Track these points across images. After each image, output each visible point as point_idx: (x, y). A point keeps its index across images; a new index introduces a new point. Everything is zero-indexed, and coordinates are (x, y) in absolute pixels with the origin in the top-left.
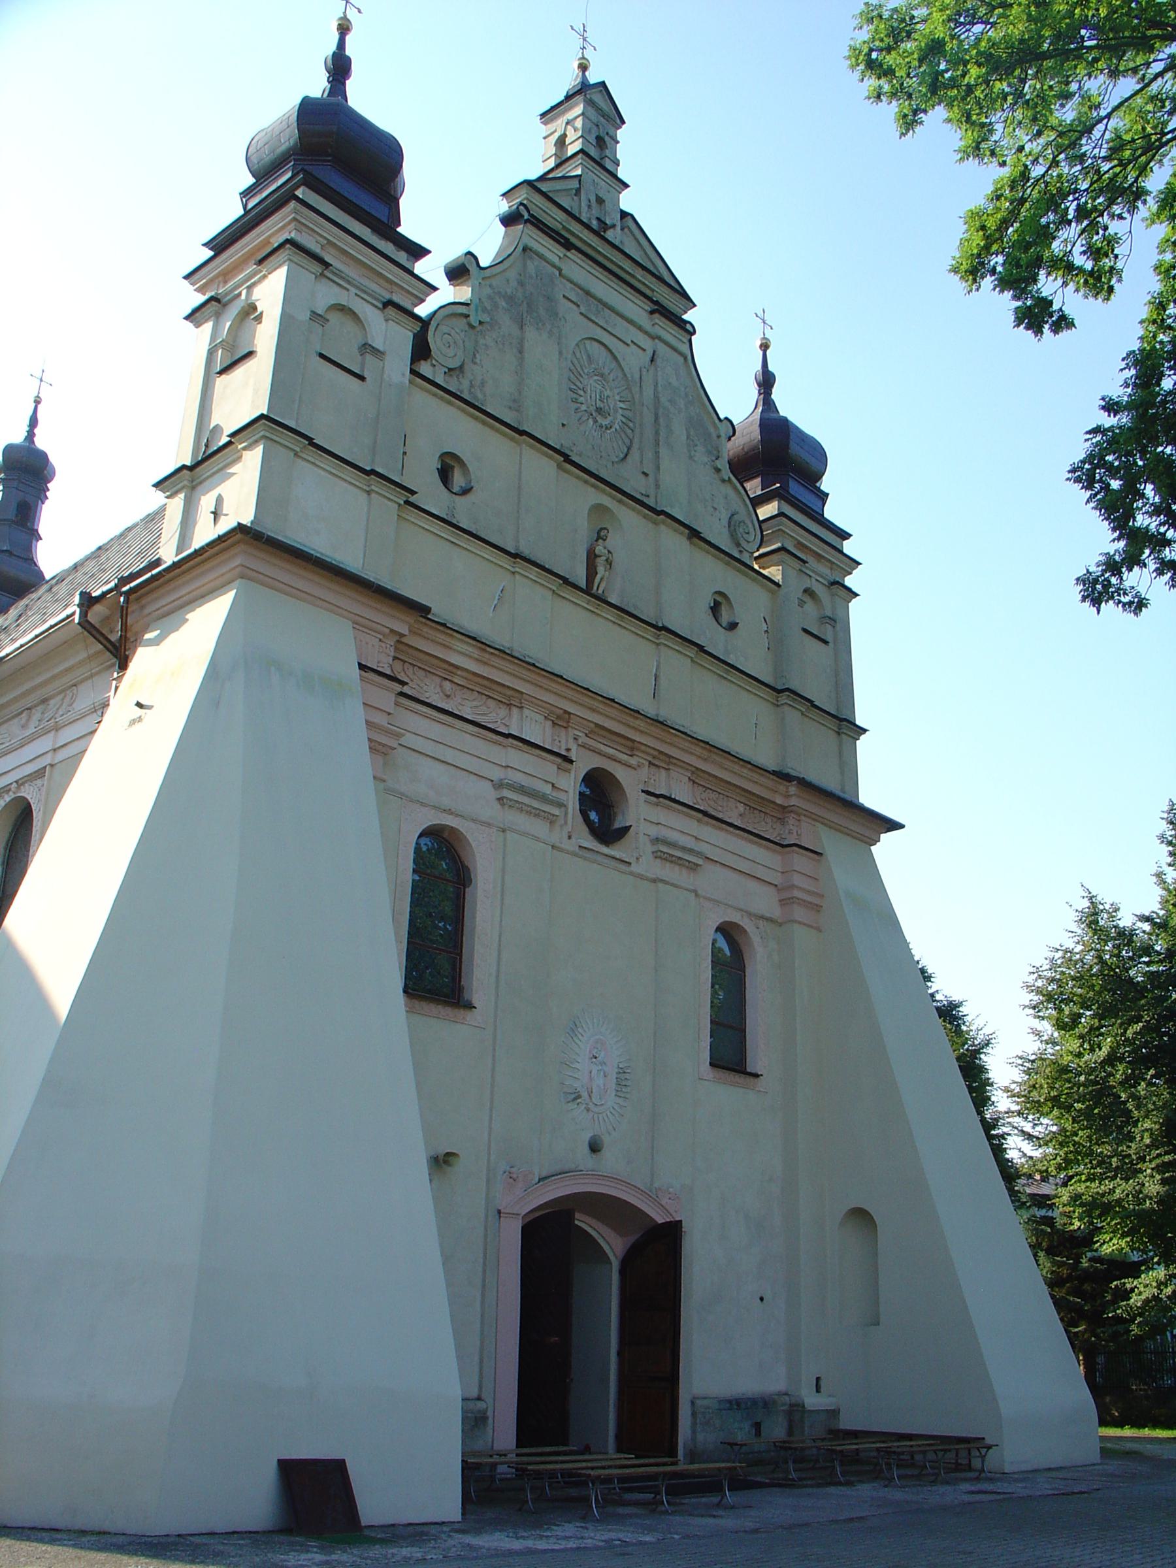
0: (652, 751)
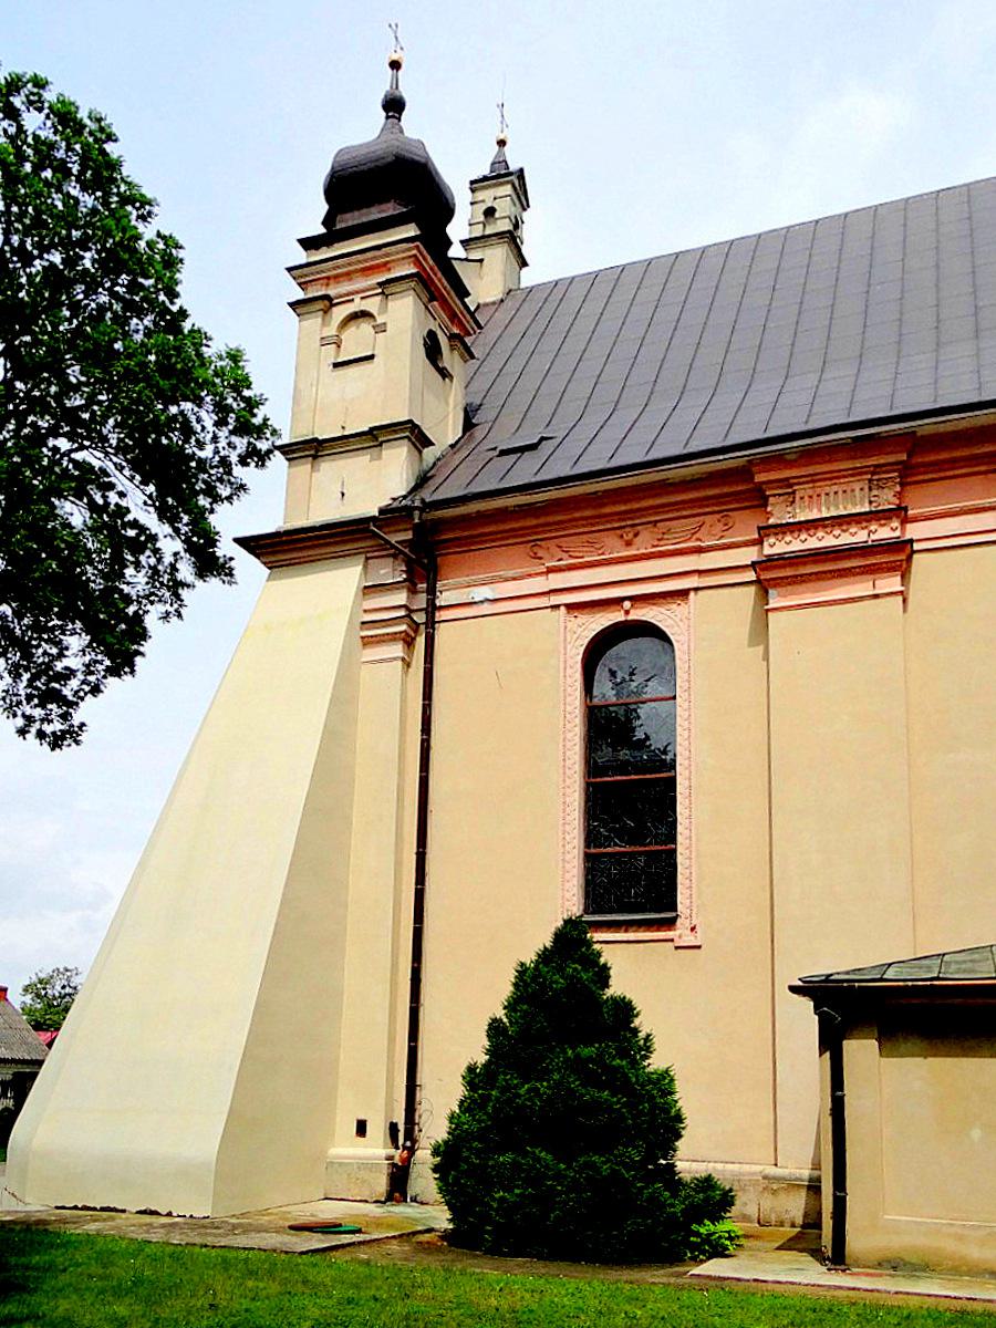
0: (895, 467)
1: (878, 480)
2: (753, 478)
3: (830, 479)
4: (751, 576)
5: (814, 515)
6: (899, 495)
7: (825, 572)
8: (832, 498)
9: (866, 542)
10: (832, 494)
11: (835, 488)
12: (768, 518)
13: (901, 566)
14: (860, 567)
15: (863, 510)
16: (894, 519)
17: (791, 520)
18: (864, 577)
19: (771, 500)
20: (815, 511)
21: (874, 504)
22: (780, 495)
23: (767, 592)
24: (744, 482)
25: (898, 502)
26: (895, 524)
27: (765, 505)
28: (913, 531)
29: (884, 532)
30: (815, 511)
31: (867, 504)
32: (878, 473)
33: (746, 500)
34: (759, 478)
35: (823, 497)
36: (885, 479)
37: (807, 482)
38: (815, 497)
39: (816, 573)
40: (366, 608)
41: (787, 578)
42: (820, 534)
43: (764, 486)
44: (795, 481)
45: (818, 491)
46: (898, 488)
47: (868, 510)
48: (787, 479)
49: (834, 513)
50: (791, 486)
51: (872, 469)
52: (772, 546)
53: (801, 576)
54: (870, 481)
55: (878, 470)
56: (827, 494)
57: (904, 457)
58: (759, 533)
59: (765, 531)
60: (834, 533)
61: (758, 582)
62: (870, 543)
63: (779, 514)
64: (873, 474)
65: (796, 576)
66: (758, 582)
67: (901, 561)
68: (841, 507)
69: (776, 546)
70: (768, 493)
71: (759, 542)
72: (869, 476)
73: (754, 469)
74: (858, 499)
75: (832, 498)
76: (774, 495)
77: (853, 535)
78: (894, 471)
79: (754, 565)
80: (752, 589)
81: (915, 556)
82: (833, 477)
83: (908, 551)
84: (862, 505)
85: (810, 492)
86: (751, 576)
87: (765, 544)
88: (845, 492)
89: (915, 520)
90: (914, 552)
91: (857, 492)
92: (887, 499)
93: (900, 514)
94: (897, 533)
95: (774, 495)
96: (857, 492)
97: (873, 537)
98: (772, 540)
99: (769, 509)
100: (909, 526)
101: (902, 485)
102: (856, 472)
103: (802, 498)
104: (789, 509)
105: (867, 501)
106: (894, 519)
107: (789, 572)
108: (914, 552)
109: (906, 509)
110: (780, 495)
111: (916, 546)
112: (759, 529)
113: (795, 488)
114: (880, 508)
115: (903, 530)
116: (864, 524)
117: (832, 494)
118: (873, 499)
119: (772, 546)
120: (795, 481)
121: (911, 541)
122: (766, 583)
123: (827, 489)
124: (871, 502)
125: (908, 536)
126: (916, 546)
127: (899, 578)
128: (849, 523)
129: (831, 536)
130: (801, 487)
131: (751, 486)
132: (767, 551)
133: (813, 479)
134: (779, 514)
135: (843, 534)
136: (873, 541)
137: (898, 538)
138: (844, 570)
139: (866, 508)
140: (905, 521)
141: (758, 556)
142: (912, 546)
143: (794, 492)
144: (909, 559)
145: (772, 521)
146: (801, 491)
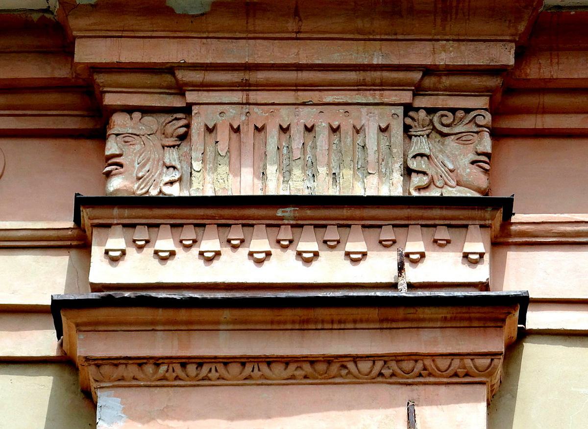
0: (476, 82)
1: (431, 111)
2: (72, 54)
3: (297, 87)
4: (42, 341)
5: (246, 184)
6: (486, 162)
7: (269, 361)
8: (297, 145)
9: (394, 286)
10: (297, 132)
11: (307, 115)
12: (108, 175)
13: (488, 371)
14: (373, 358)
15: (384, 192)
16: (474, 230)
17: (174, 191)
18: (383, 391)
19: (120, 123)
20: (247, 173)
21: (416, 180)
22: (146, 111)
23: (89, 399)
24: (43, 53)
25: (482, 181)
26: (477, 245)
27: (100, 135)
28: (527, 273)
29: (445, 266)
30: (247, 173)
31: (397, 177)
32: (435, 91)
33: (42, 110)
34: (91, 51)
35: (273, 135)
36: (453, 111)
37: (231, 87)
38: (248, 133)
39: (243, 361)
40: (413, 280)
41: (157, 361)
42: (260, 244)
43: (100, 79)
44: (196, 77)
45: (259, 115)
46: (486, 144)
47: (398, 192)
48: (169, 69)
49: (299, 186)
50: (180, 90)
51: (417, 76)
52: (114, 260)
53: (200, 361)
54: (408, 108)
55: (429, 82)
56: (284, 130)
57: (509, 59)
58: (77, 219)
59: (96, 214)
60: (302, 246)
61: (63, 362)
62: (403, 292)
63: (141, 165)
64: (418, 90)
65: (184, 362)
66: (63, 362)
67: (493, 355)
68: (323, 170)
69: (128, 263)
70: (110, 100)
71: (78, 243)
72: (406, 97)
73: (76, 24)
74: (372, 156)
75: (297, 145)
76: (129, 110)
77: (356, 259)
78: (478, 92)
79: (58, 310)
80: (42, 385)
81: (530, 349)
82: (304, 81)
83: (511, 325)
84: (384, 176)
85: (234, 115)
86: (42, 341)
87: (97, 252)
88: (335, 130)
89: (533, 241)
90: (524, 334)
91: (372, 137)
92: (455, 167)
93: (490, 215)
94: (481, 273)
95: (129, 110)
96: (372, 137)
97: (413, 274)
98: (116, 242)
99: (112, 147)
100: (515, 259)
101: (497, 135)
102: (369, 79)
103: (210, 130)
104: (172, 156)
105: (397, 167)
106: (474, 230)
107: (161, 346)
108: (524, 334)
109: (506, 206)
110: (146, 111)
111: (536, 319)
112: (81, 202)
113: (191, 97)
114: (434, 193)
115: (497, 268)
116: (387, 234)
117: (297, 132)
118: (413, 165)
119: (114, 260)
120: (196, 77)
121: (522, 302)
122: (90, 372)
123: (285, 116)
124: (408, 172)
125: (510, 286)
126: (536, 319)
127: (483, 406)
128: (402, 226)
129: (291, 253)
130: (214, 97)
131: (61, 72)
132: (101, 272)
133: (246, 79)
134: (141, 165)
135: (324, 255)
136: (411, 286)
137: (485, 286)
138: (329, 360)
139: (393, 187)
140: (503, 240)
141: (404, 191)
142: (522, 319)
143: (187, 110)
144: (513, 348)
145: (117, 185)
146: (212, 110)
